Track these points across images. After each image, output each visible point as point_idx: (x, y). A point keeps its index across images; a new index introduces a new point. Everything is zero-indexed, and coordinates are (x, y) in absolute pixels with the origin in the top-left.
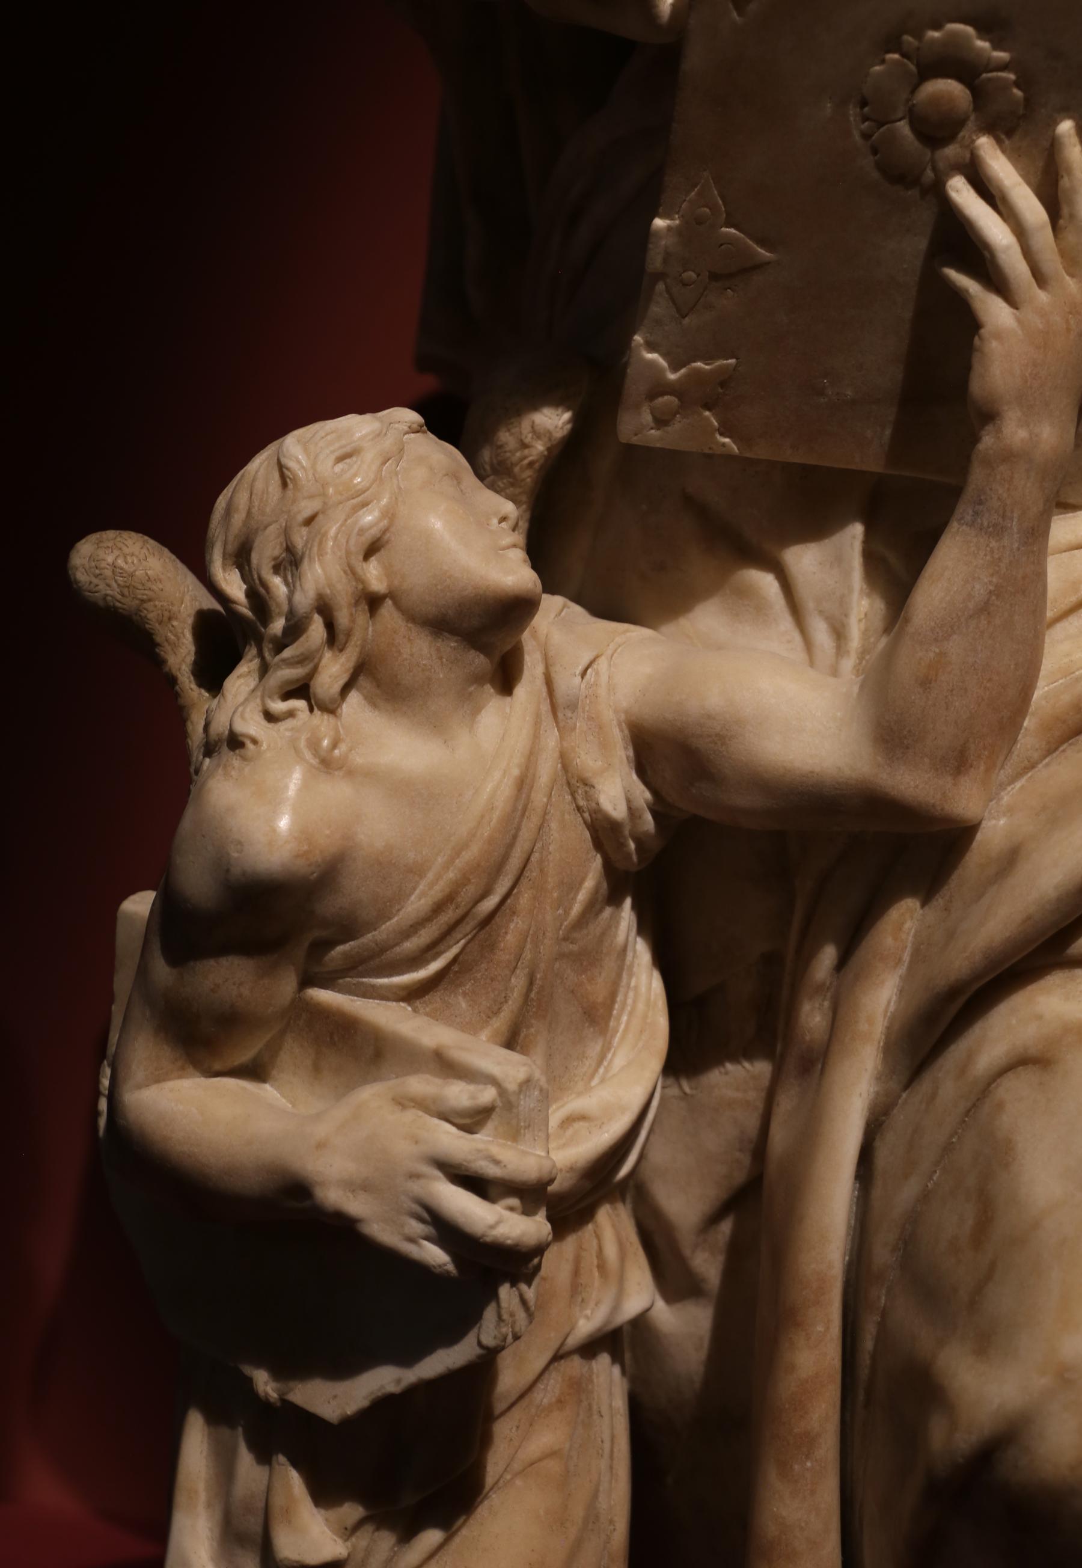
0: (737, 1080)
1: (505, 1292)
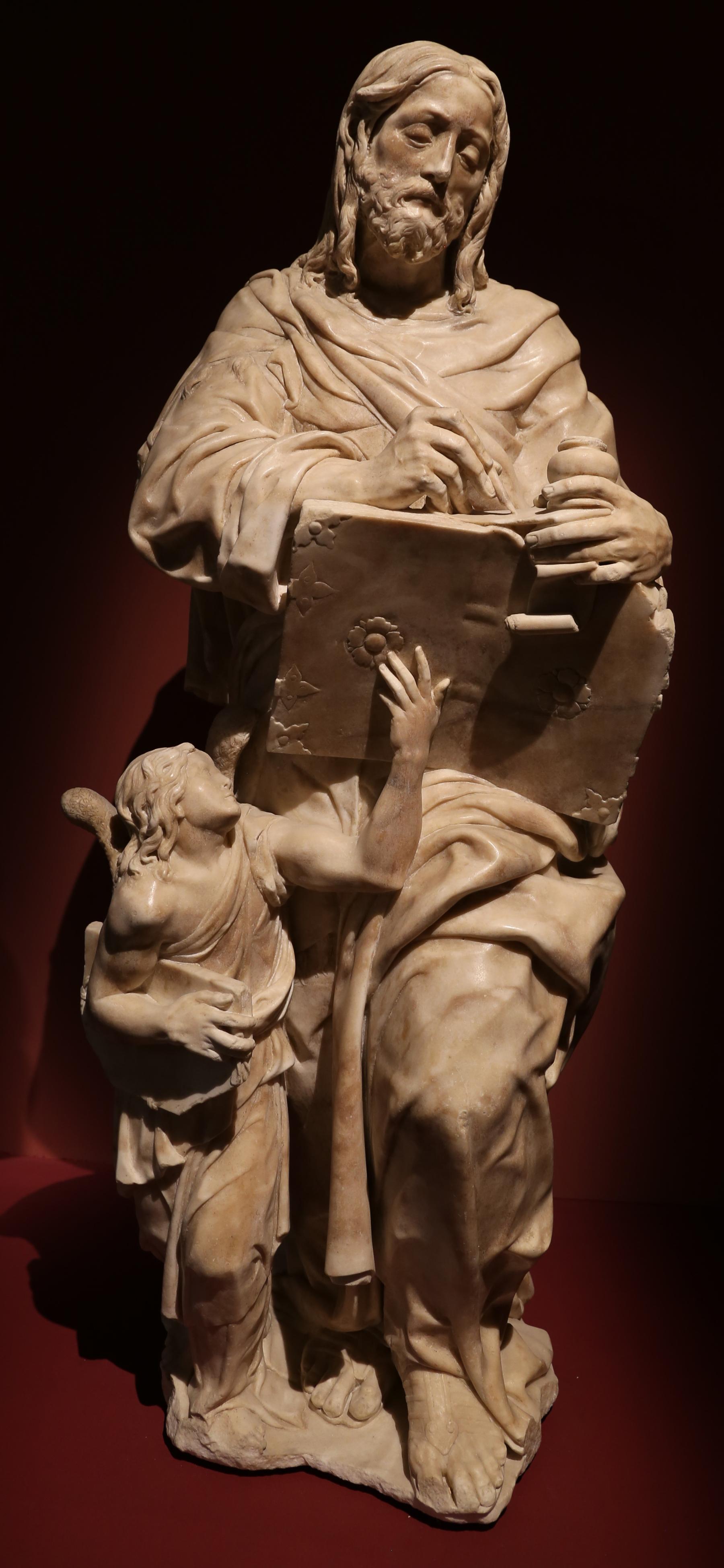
0: (322, 980)
1: (239, 1065)
